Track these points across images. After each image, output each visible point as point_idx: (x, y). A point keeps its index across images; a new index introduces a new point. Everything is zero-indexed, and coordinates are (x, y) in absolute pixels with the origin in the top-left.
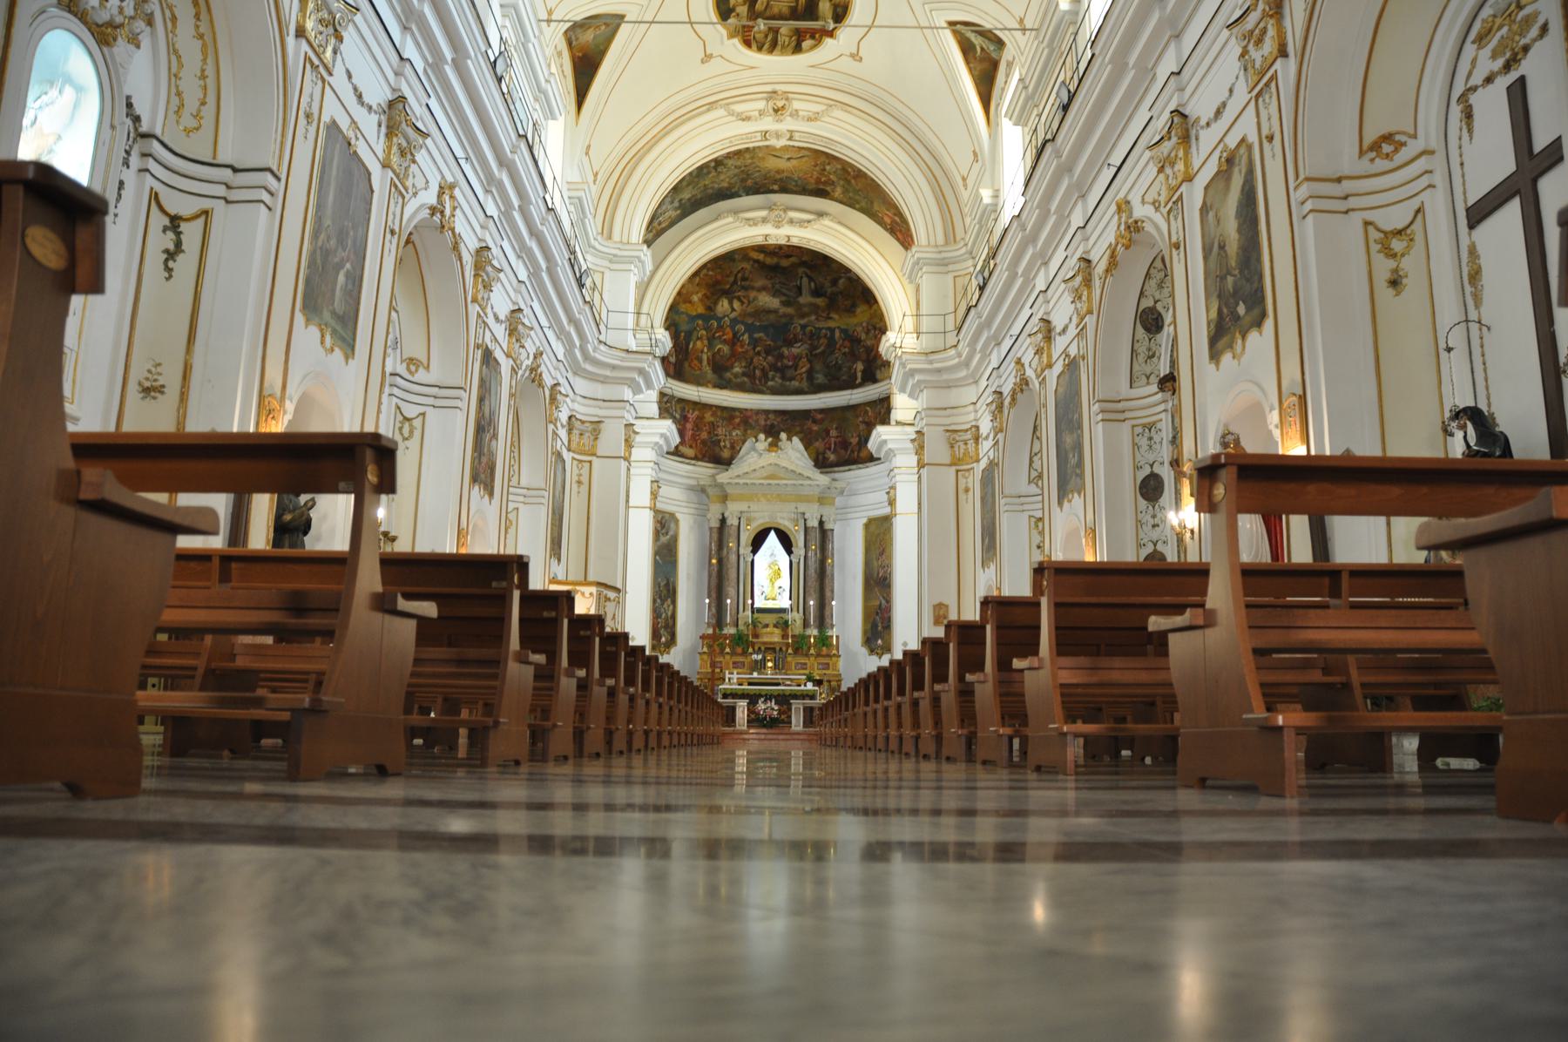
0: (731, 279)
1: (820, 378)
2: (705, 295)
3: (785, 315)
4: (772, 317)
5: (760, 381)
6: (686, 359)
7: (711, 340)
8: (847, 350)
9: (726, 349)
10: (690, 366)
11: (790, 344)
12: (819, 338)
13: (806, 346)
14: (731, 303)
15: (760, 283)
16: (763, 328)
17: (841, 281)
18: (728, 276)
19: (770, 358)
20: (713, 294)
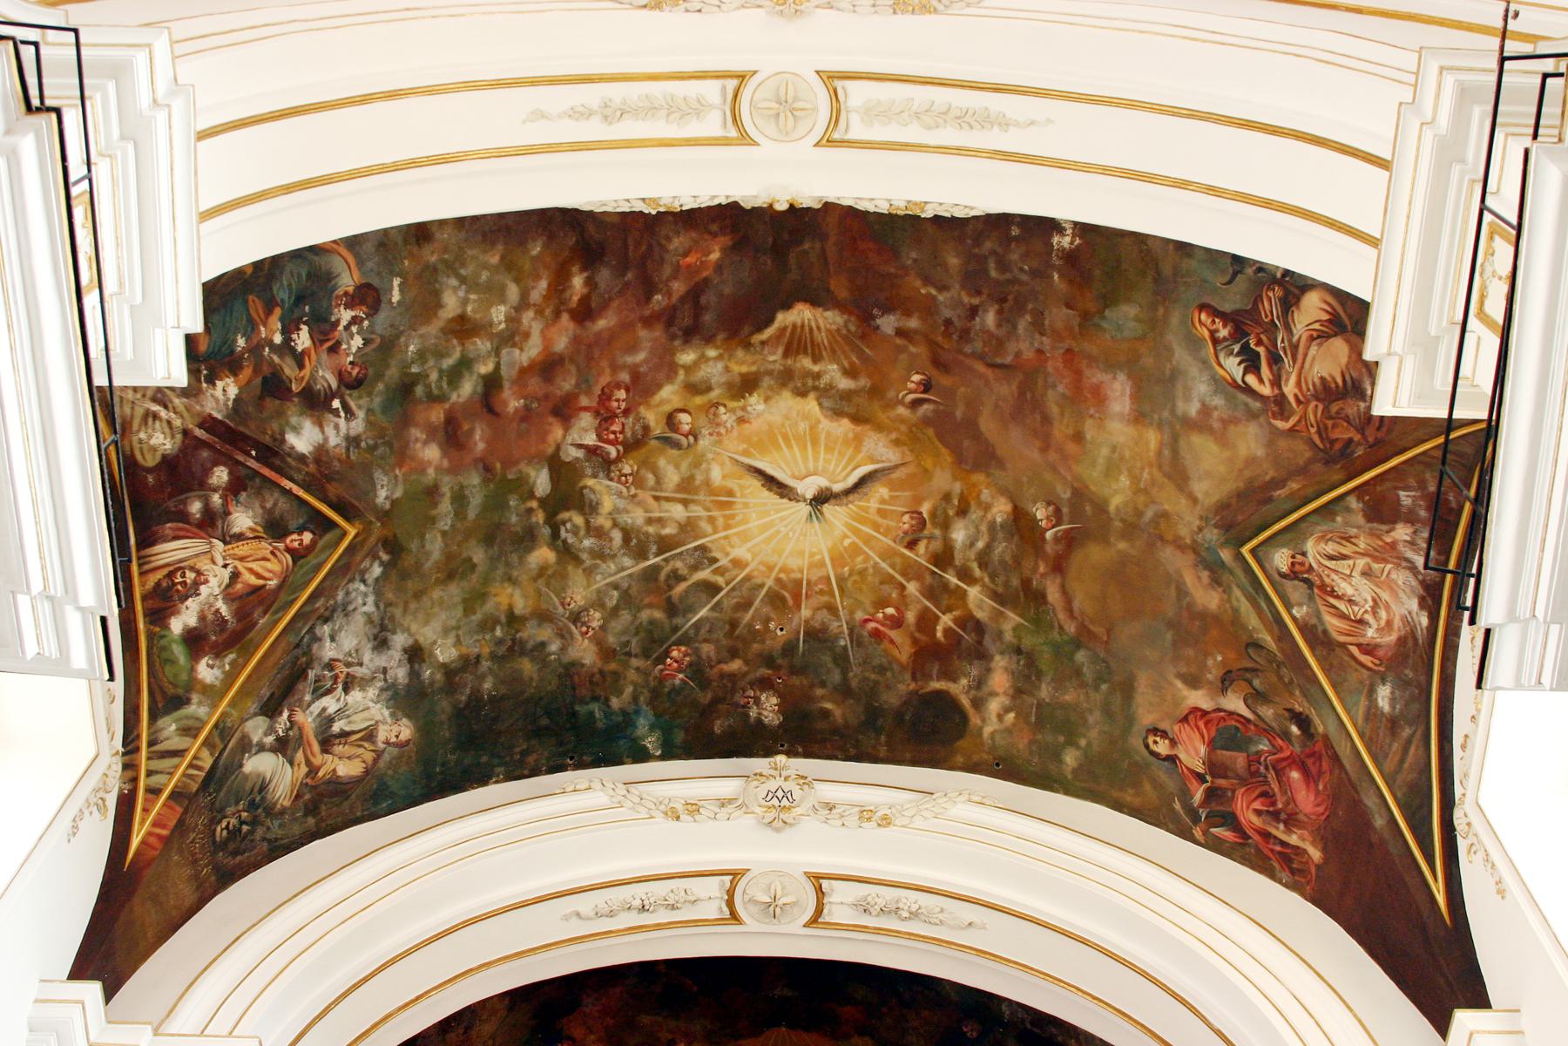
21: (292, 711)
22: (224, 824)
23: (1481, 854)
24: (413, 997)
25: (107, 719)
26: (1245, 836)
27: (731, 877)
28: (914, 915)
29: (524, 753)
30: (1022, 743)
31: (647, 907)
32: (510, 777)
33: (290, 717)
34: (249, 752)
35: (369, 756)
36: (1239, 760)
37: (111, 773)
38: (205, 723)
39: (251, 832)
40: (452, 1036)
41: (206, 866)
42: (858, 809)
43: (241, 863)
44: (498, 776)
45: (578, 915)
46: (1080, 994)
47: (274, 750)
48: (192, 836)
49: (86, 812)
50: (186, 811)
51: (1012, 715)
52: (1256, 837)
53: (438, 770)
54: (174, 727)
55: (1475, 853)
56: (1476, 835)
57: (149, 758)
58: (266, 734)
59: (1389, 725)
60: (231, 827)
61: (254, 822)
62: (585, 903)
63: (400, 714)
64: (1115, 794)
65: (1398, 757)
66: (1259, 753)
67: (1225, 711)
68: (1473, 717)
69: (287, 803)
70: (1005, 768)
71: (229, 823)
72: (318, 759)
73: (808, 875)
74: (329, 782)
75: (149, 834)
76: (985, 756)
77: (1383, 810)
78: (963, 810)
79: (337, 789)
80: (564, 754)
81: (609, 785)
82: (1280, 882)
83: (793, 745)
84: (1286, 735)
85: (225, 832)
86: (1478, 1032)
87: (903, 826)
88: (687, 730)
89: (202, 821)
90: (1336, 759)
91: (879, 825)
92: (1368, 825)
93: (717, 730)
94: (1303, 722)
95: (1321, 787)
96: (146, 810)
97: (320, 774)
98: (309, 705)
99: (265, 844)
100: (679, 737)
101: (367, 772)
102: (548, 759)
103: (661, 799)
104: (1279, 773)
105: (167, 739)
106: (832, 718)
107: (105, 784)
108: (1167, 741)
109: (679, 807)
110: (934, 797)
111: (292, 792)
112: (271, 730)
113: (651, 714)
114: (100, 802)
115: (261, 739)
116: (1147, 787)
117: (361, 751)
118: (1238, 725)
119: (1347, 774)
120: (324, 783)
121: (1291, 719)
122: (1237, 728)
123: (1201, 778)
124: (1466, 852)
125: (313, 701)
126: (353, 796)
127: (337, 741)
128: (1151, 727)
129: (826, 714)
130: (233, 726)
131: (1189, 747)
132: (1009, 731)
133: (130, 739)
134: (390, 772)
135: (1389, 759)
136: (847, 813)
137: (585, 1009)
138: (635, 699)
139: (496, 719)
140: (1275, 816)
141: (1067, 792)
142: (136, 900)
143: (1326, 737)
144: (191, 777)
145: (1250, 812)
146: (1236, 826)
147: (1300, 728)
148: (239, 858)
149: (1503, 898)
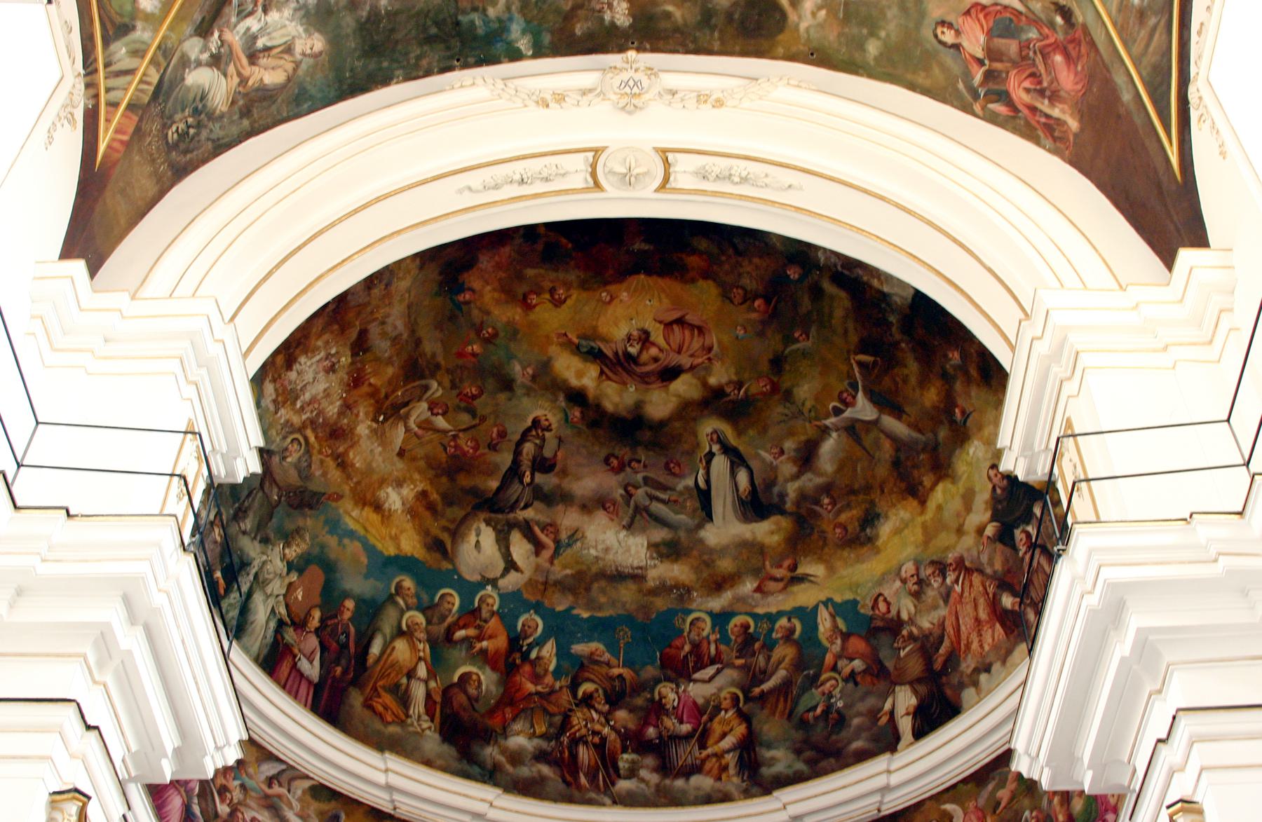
0: (505, 459)
1: (780, 759)
2: (424, 494)
3: (663, 588)
4: (627, 594)
5: (593, 778)
6: (357, 682)
7: (441, 643)
8: (858, 664)
9: (487, 679)
10: (368, 705)
11: (679, 670)
12: (769, 646)
13: (730, 674)
14: (503, 541)
15: (589, 482)
16: (601, 628)
17: (828, 446)
18: (493, 447)
19: (622, 715)
20: (449, 500)
21: (221, 31)
22: (174, 128)
23: (1208, 122)
24: (339, 260)
25: (67, 47)
26: (1016, 110)
27: (593, 153)
28: (744, 180)
29: (419, 58)
30: (832, 35)
31: (525, 180)
32: (409, 78)
33: (220, 37)
34: (189, 67)
35: (290, 67)
36: (1012, 47)
37: (75, 92)
38: (149, 46)
39: (197, 134)
40: (376, 292)
41: (163, 163)
42: (695, 94)
43: (191, 160)
44: (398, 77)
45: (470, 189)
46: (879, 241)
47: (209, 65)
48: (148, 139)
49: (59, 125)
50: (141, 120)
51: (823, 13)
52: (1025, 112)
53: (347, 75)
54: (124, 50)
55: (1204, 121)
56: (1206, 107)
57: (106, 78)
58: (202, 52)
59: (1138, 15)
60: (180, 130)
61: (199, 126)
62: (475, 179)
63: (312, 30)
64: (909, 76)
65: (1144, 43)
66: (1029, 41)
67: (1001, 5)
68: (1208, 7)
69: (225, 109)
70: (819, 57)
71: (178, 128)
72: (247, 70)
73: (656, 150)
74: (257, 90)
75: (113, 140)
76: (801, 48)
77: (1130, 86)
78: (783, 92)
79: (265, 95)
80: (451, 57)
81: (490, 81)
82: (1044, 147)
83: (642, 43)
84: (1052, 25)
85: (175, 136)
86: (1197, 267)
87: (734, 107)
88: (552, 33)
89: (155, 127)
90: (1092, 44)
91: (713, 106)
92: (1118, 99)
93: (578, 32)
94: (1066, 13)
95: (1079, 68)
96: (108, 121)
97: (250, 83)
98: (235, 26)
99: (210, 143)
100: (547, 39)
101: (289, 79)
102: (439, 61)
103: (533, 91)
104: (1045, 57)
105: (119, 61)
106: (673, 19)
107: (71, 100)
108: (953, 32)
109: (548, 97)
110: (759, 82)
111: (228, 99)
112: (205, 48)
113: (522, 21)
114: (69, 116)
115: (198, 56)
116: (936, 71)
117: (282, 62)
118: (1012, 17)
119: (1101, 57)
120: (253, 91)
121: (1056, 11)
122: (1011, 20)
123: (980, 62)
124: (1196, 122)
125: (238, 22)
126: (279, 100)
127: (261, 55)
128: (939, 20)
129: (668, 15)
130: (173, 47)
131: (971, 36)
132: (821, 26)
133: (89, 63)
134: (308, 79)
135: (1136, 45)
136: (686, 97)
137: (481, 265)
138: (508, 8)
139: (392, 30)
140: (1042, 93)
141: (871, 76)
142: (108, 194)
143: (1085, 27)
144: (142, 91)
145: (1021, 90)
146: (1010, 103)
147: (1063, 17)
148: (189, 156)
149: (1224, 158)
